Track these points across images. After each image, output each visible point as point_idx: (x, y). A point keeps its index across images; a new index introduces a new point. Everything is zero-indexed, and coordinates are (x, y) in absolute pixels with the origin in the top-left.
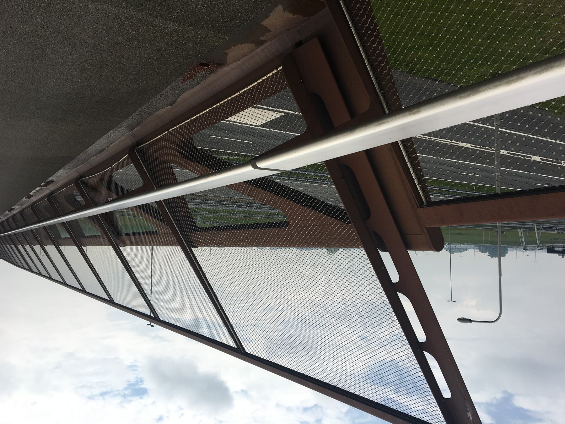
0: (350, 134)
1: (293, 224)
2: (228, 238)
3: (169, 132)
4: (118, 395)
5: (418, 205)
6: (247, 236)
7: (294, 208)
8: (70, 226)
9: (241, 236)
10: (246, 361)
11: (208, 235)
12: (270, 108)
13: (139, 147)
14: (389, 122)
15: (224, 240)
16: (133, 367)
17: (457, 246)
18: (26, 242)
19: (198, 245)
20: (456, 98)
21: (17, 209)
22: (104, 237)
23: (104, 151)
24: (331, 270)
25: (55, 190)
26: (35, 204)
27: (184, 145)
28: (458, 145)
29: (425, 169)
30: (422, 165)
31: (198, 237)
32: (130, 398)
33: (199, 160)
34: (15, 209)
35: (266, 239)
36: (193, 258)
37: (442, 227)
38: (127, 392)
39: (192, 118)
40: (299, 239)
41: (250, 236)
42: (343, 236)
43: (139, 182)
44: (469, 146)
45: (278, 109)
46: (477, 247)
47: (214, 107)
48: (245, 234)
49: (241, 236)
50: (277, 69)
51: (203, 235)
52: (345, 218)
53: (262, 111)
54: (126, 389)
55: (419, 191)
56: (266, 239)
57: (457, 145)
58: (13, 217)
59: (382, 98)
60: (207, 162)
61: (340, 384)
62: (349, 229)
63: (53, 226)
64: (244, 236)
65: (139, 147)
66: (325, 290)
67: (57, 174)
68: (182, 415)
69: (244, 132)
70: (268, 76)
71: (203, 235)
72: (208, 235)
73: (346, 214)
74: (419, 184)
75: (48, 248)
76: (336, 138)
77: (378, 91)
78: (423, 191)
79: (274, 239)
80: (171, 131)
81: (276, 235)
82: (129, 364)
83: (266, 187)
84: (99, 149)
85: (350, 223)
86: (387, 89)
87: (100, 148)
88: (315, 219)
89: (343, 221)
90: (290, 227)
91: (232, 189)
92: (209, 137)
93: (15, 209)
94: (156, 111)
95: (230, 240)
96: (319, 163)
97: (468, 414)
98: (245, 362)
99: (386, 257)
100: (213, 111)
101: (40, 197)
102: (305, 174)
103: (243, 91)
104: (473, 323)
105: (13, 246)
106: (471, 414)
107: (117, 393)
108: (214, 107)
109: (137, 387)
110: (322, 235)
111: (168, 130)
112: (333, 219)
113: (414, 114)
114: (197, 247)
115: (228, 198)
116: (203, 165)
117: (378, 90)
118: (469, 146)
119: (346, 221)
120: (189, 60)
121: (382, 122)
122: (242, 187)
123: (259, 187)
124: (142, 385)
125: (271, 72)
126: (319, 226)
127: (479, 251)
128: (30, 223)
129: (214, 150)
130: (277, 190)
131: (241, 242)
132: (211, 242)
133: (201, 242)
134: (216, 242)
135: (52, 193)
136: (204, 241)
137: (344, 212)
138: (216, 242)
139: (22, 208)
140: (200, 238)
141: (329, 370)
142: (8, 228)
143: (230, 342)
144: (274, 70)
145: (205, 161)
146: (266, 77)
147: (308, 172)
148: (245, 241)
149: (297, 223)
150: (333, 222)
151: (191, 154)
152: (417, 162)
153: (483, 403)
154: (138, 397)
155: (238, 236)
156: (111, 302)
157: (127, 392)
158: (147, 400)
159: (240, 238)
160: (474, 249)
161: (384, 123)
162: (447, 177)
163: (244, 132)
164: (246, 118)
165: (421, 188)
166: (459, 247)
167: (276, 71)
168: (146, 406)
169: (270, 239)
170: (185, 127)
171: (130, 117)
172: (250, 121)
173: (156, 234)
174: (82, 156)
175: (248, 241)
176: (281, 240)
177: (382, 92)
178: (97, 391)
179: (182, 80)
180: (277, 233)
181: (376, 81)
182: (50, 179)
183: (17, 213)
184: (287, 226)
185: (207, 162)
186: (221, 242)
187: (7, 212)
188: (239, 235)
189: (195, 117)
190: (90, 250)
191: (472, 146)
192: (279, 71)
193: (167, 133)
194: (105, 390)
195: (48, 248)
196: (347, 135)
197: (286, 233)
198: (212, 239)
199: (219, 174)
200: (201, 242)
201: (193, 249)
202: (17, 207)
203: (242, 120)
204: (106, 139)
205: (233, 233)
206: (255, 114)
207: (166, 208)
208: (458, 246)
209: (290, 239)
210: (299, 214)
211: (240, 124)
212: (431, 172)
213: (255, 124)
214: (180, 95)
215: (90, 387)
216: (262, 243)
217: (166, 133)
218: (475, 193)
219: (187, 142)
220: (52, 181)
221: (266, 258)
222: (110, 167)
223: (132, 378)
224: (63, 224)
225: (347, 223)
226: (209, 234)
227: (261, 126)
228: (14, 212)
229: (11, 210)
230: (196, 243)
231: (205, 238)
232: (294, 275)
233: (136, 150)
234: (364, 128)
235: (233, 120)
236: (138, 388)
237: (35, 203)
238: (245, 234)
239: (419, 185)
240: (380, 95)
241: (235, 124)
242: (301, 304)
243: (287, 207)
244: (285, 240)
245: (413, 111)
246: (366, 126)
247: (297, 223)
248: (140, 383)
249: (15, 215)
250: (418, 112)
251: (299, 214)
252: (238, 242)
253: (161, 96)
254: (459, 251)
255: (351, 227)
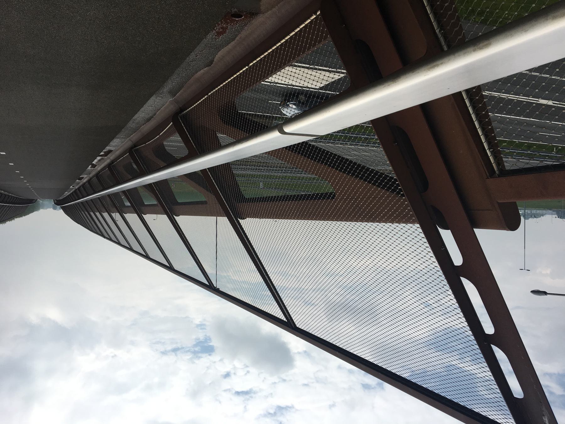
0: (393, 84)
1: (339, 196)
2: (273, 210)
3: (208, 96)
4: (189, 351)
5: (488, 174)
6: (292, 209)
7: (340, 178)
8: (131, 194)
9: (286, 208)
10: (297, 336)
11: (254, 206)
12: (330, 69)
13: (182, 114)
14: (445, 63)
15: (269, 212)
16: (201, 326)
17: (532, 211)
18: (97, 211)
19: (246, 216)
20: (547, 20)
21: (86, 178)
22: (160, 208)
23: (152, 119)
24: (382, 248)
25: (114, 159)
26: (100, 173)
27: (224, 110)
28: (538, 102)
29: (498, 130)
30: (494, 124)
31: (244, 208)
32: (200, 355)
33: (240, 126)
34: (83, 178)
35: (312, 212)
36: (240, 230)
37: (518, 203)
38: (197, 349)
39: (230, 80)
40: (346, 213)
41: (295, 209)
42: (395, 211)
43: (186, 152)
44: (550, 103)
45: (340, 70)
46: (555, 213)
47: (251, 64)
48: (290, 207)
49: (286, 208)
50: (315, 13)
51: (249, 207)
52: (398, 190)
53: (317, 72)
54: (195, 346)
55: (490, 157)
56: (312, 212)
57: (536, 102)
58: (84, 185)
59: (442, 40)
60: (247, 128)
61: (405, 341)
62: (403, 203)
63: (116, 194)
64: (289, 208)
65: (182, 114)
66: (376, 270)
67: (112, 143)
68: (248, 372)
69: (274, 92)
70: (306, 23)
71: (249, 207)
72: (254, 206)
73: (398, 185)
74: (489, 149)
75: (113, 215)
76: (375, 90)
77: (437, 31)
78: (495, 158)
79: (320, 212)
80: (211, 94)
81: (322, 208)
82: (199, 323)
83: (309, 155)
84: (147, 117)
85: (403, 195)
86: (448, 28)
87: (147, 116)
88: (363, 190)
89: (395, 193)
90: (337, 199)
91: (271, 155)
92: (268, 103)
93: (83, 178)
94: (194, 74)
95: (275, 212)
96: (363, 123)
97: (544, 418)
98: (296, 337)
99: (447, 236)
100: (250, 70)
101: (103, 166)
102: (358, 137)
103: (280, 44)
104: (548, 296)
105: (86, 213)
106: (548, 419)
107: (188, 349)
108: (251, 64)
109: (206, 345)
110: (372, 208)
111: (207, 94)
112: (384, 191)
113: (481, 48)
114: (243, 219)
115: (277, 163)
116: (244, 131)
117: (437, 29)
118: (550, 103)
119: (399, 193)
120: (216, 10)
121: (435, 64)
122: (282, 153)
123: (302, 154)
124: (210, 343)
125: (309, 18)
126: (369, 198)
127: (557, 217)
128: (97, 191)
129: (268, 115)
130: (321, 157)
131: (286, 215)
132: (256, 213)
133: (247, 214)
134: (261, 214)
135: (112, 162)
136: (250, 212)
137: (397, 183)
138: (261, 214)
139: (90, 177)
140: (246, 210)
141: (399, 325)
142: (81, 196)
143: (281, 316)
144: (312, 15)
145: (245, 126)
146: (304, 25)
147: (328, 140)
148: (290, 213)
149: (344, 196)
150: (384, 194)
151: (229, 119)
152: (487, 120)
153: (555, 374)
154: (207, 354)
155: (282, 209)
156: (170, 268)
157: (197, 349)
158: (216, 357)
159: (285, 210)
160: (552, 214)
161: (438, 65)
162: (518, 136)
163: (274, 92)
164: (307, 80)
165: (491, 153)
166: (535, 213)
167: (315, 16)
168: (215, 362)
169: (316, 212)
170: (223, 90)
171: (170, 81)
172: (312, 84)
173: (205, 204)
174: (131, 125)
175: (293, 213)
176: (327, 214)
177: (443, 31)
178: (169, 348)
179: (216, 35)
180: (323, 206)
181: (431, 10)
182: (108, 148)
183: (86, 182)
184: (333, 198)
185: (247, 128)
186: (266, 213)
187: (77, 180)
188: (283, 207)
189: (232, 78)
190: (148, 218)
191: (553, 103)
192: (318, 15)
193: (207, 97)
194: (179, 346)
195: (128, 216)
196: (389, 85)
197: (332, 206)
198: (257, 210)
199: (246, 142)
200: (247, 214)
201: (240, 221)
202: (86, 176)
203: (287, 81)
204: (151, 106)
205: (278, 205)
206: (305, 75)
207: (212, 178)
208: (534, 211)
209: (337, 213)
210: (346, 185)
211: (285, 86)
212: (506, 132)
213: (302, 85)
214: (217, 54)
215: (164, 343)
216: (303, 216)
217: (206, 97)
218: (555, 155)
219: (226, 106)
220: (110, 151)
221: (318, 230)
222: (158, 135)
223: (201, 336)
224: (149, 187)
225: (400, 195)
226: (254, 205)
227: (321, 88)
228: (85, 181)
229: (81, 179)
230: (243, 214)
231: (250, 209)
232: (343, 252)
233: (180, 117)
234: (411, 74)
235: (294, 85)
236: (207, 346)
237: (99, 172)
238: (290, 207)
239: (489, 150)
240: (440, 36)
241: (294, 87)
242: (357, 276)
243: (332, 177)
244: (331, 214)
245: (479, 44)
246: (413, 72)
247: (344, 196)
248: (208, 341)
249: (85, 184)
250: (487, 46)
251: (346, 185)
252: (283, 215)
253: (196, 56)
254: (535, 217)
255: (405, 200)
